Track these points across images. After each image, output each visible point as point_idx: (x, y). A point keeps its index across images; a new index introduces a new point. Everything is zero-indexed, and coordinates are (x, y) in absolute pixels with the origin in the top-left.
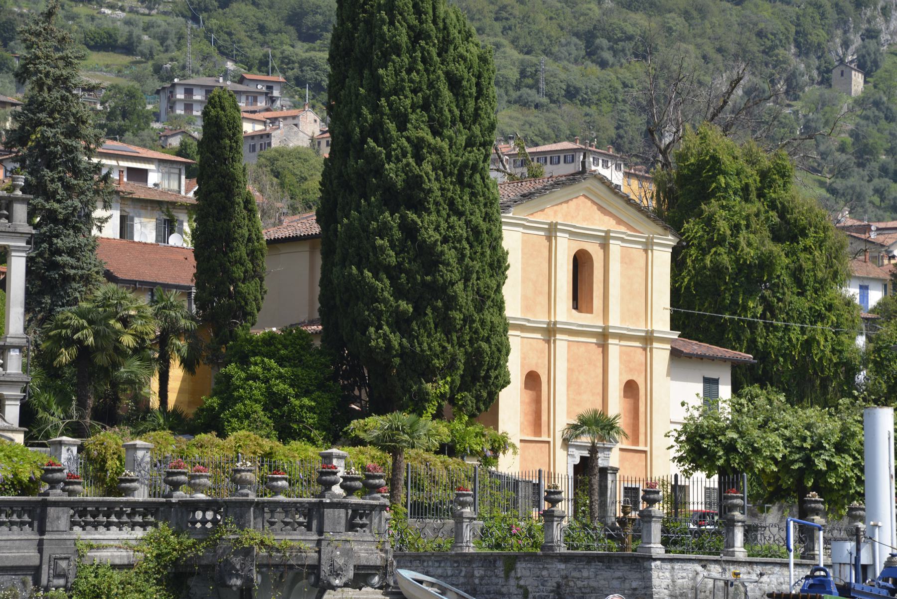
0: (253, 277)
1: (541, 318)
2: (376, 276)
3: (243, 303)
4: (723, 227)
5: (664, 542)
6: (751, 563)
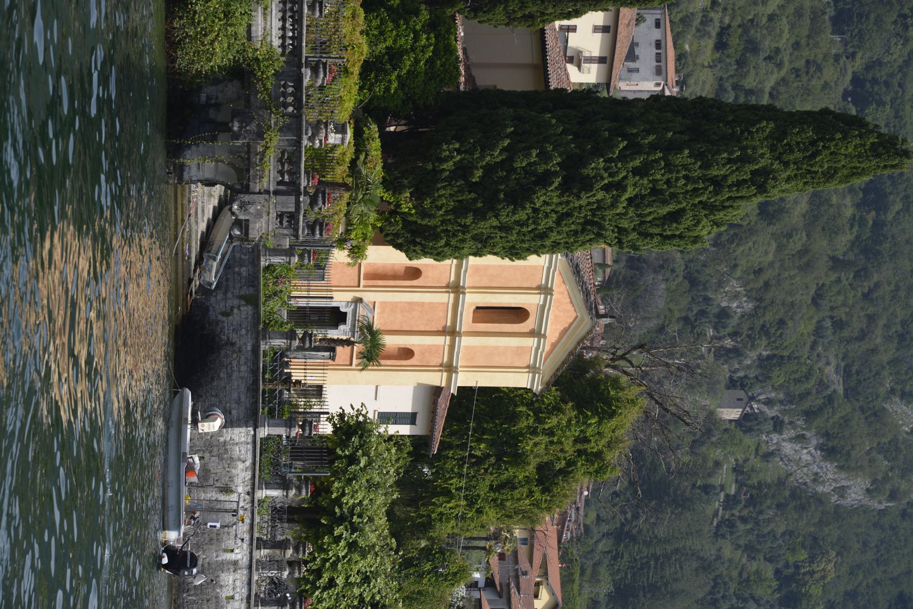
0: (509, 17)
1: (468, 281)
2: (504, 150)
3: (485, 9)
4: (553, 422)
5: (269, 438)
6: (253, 501)
